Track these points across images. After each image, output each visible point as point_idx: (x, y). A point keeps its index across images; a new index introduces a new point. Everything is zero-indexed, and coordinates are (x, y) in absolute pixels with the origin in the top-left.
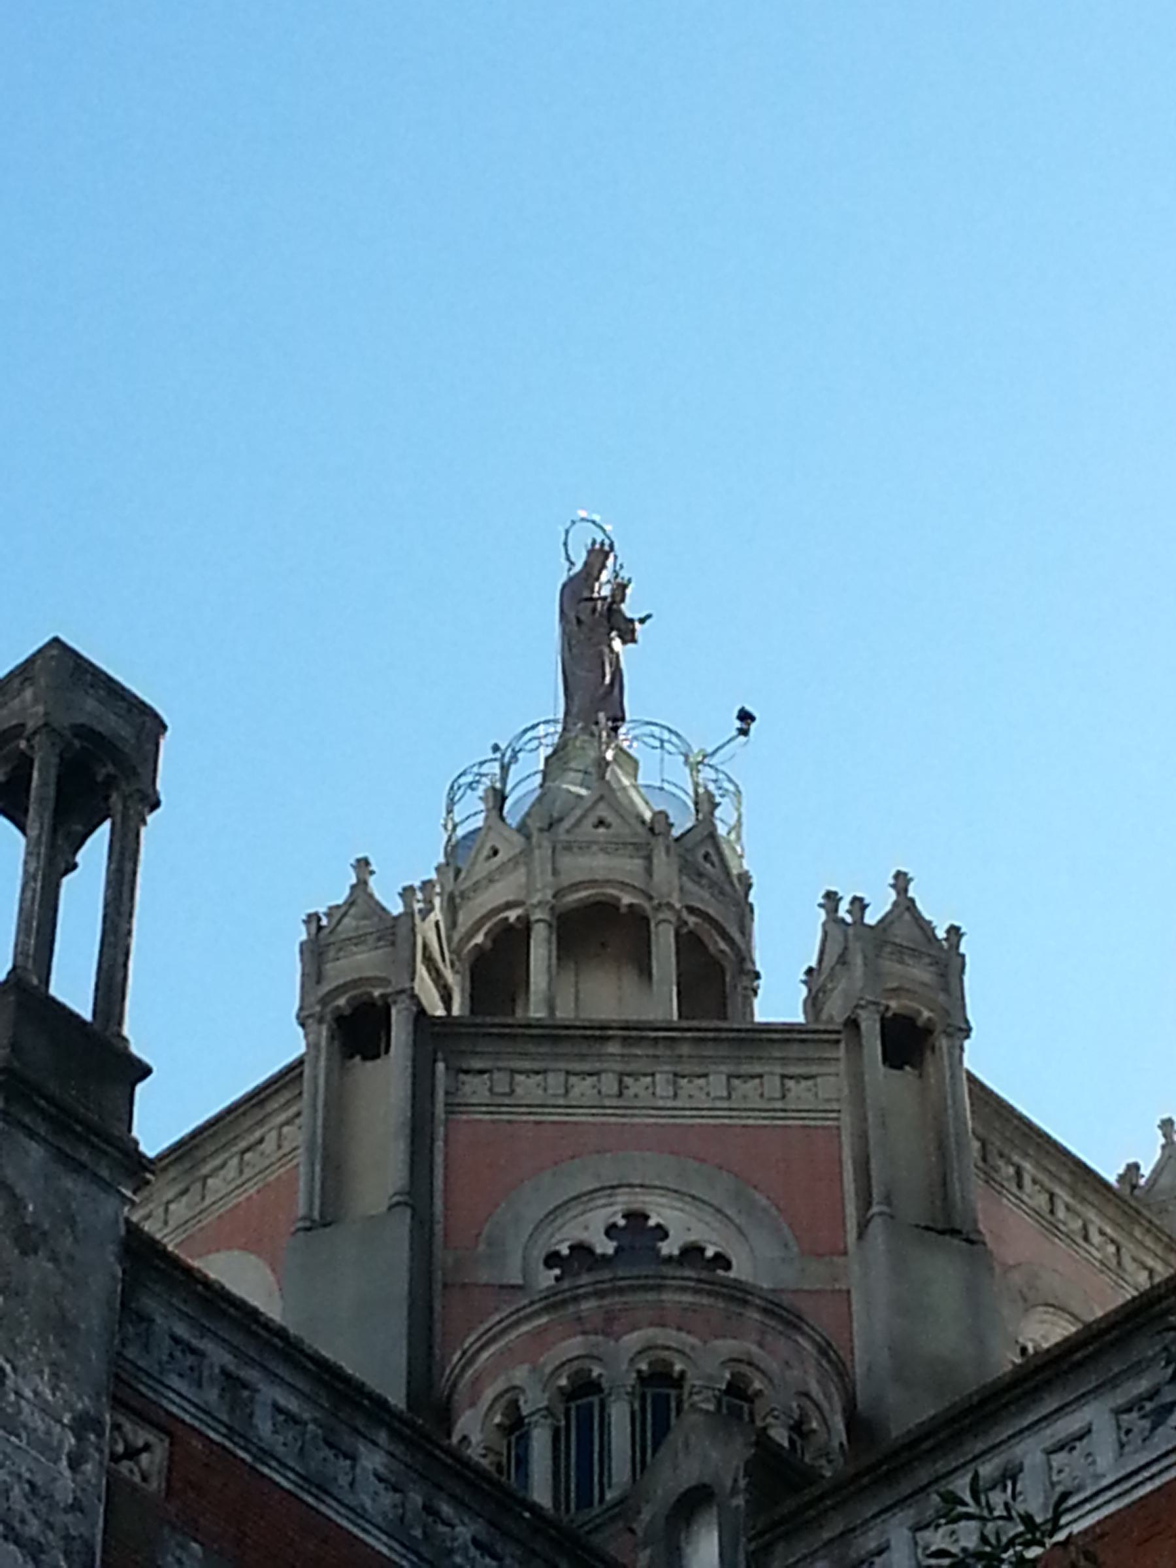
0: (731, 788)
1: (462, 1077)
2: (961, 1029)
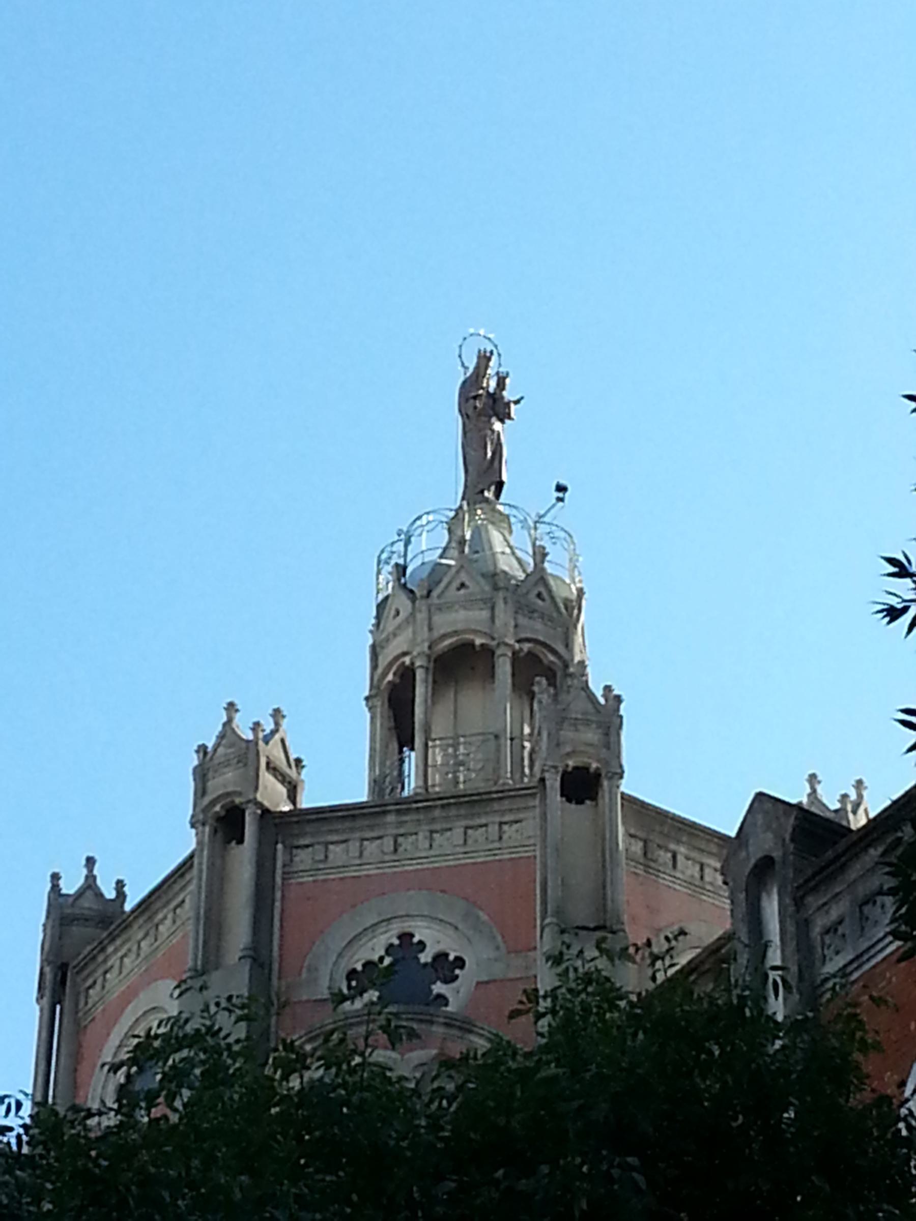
0: (562, 534)
1: (295, 851)
2: (616, 774)
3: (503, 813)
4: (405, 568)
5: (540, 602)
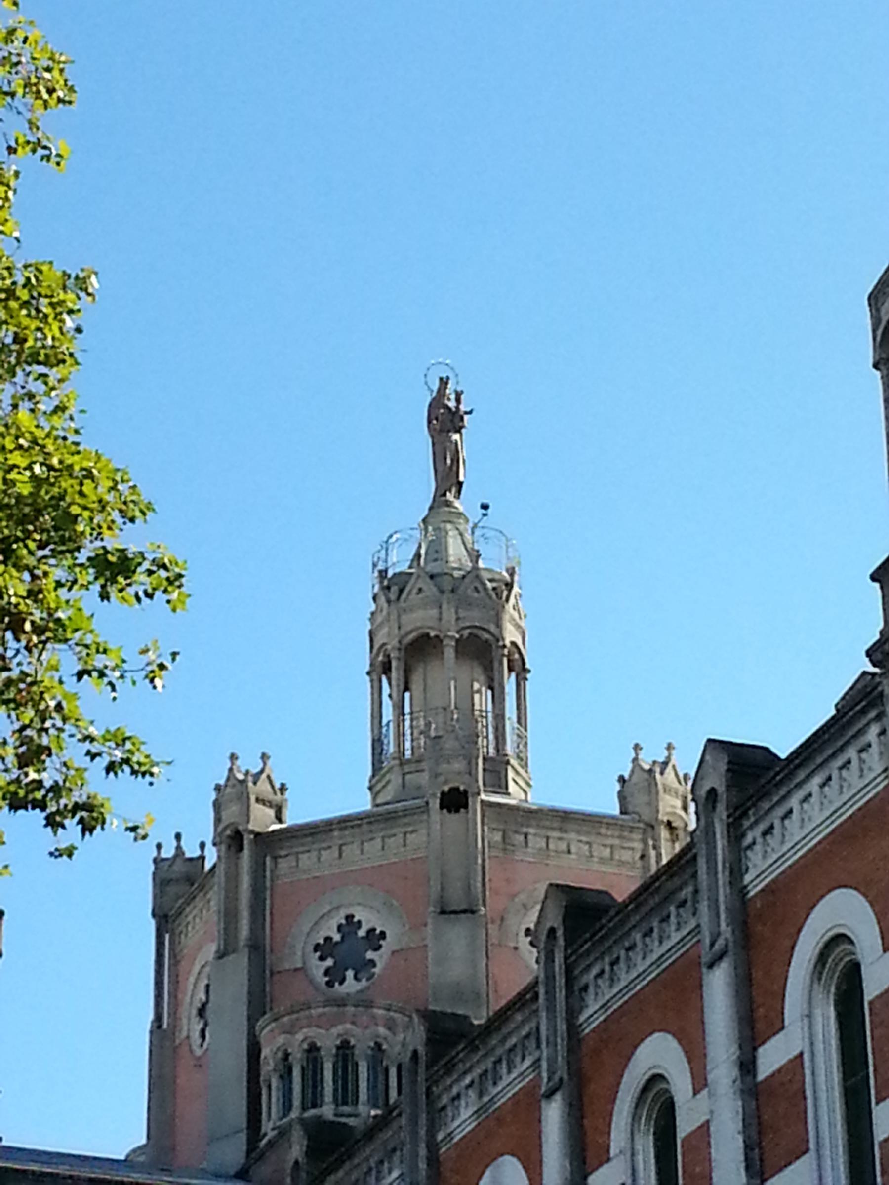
3: (406, 824)
4: (386, 571)
5: (476, 595)
